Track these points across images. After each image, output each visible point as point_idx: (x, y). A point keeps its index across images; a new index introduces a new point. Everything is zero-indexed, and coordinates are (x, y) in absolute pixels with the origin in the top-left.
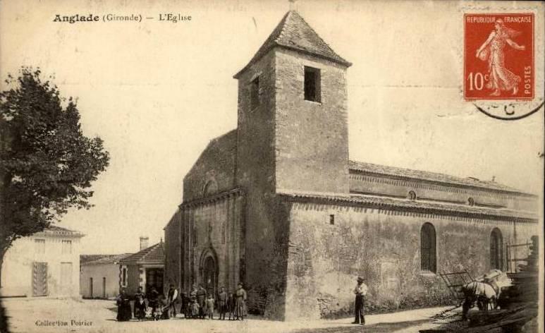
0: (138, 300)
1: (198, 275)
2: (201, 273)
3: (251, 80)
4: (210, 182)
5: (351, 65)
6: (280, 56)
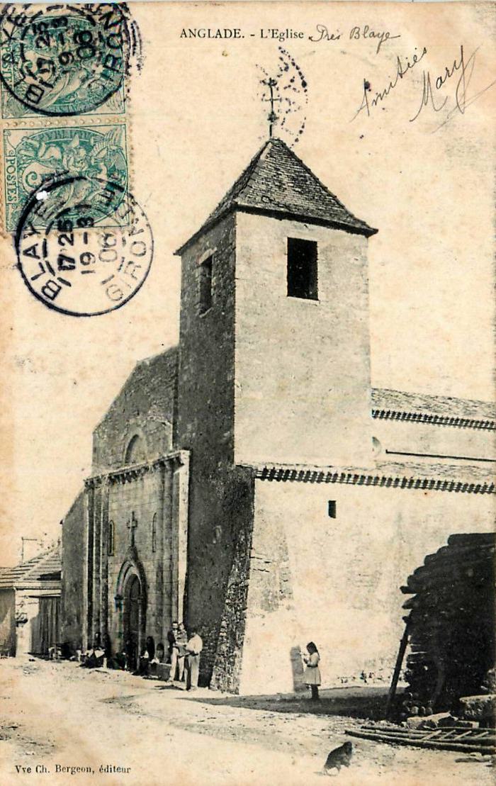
0: (108, 653)
1: (114, 609)
2: (118, 606)
3: (201, 261)
4: (136, 437)
5: (376, 231)
6: (240, 216)
